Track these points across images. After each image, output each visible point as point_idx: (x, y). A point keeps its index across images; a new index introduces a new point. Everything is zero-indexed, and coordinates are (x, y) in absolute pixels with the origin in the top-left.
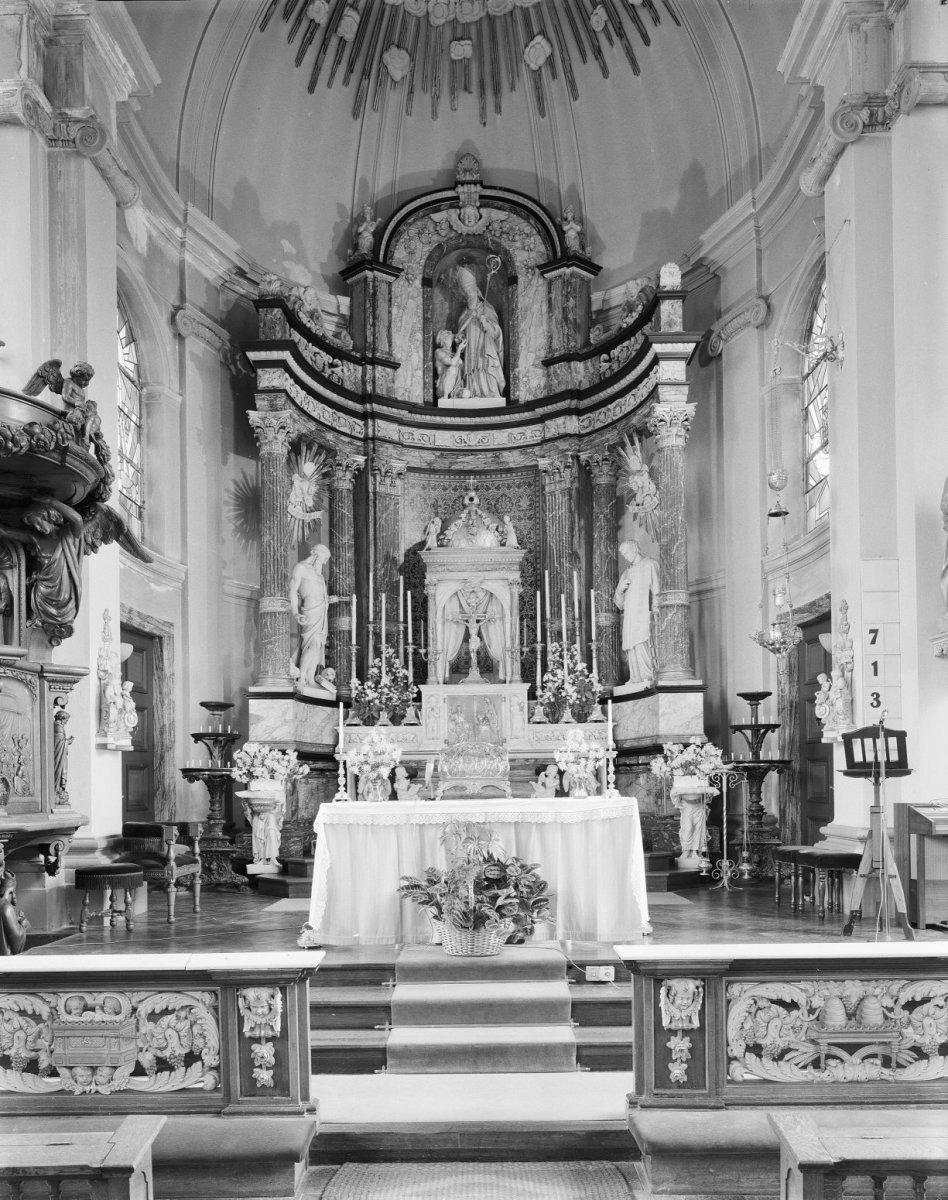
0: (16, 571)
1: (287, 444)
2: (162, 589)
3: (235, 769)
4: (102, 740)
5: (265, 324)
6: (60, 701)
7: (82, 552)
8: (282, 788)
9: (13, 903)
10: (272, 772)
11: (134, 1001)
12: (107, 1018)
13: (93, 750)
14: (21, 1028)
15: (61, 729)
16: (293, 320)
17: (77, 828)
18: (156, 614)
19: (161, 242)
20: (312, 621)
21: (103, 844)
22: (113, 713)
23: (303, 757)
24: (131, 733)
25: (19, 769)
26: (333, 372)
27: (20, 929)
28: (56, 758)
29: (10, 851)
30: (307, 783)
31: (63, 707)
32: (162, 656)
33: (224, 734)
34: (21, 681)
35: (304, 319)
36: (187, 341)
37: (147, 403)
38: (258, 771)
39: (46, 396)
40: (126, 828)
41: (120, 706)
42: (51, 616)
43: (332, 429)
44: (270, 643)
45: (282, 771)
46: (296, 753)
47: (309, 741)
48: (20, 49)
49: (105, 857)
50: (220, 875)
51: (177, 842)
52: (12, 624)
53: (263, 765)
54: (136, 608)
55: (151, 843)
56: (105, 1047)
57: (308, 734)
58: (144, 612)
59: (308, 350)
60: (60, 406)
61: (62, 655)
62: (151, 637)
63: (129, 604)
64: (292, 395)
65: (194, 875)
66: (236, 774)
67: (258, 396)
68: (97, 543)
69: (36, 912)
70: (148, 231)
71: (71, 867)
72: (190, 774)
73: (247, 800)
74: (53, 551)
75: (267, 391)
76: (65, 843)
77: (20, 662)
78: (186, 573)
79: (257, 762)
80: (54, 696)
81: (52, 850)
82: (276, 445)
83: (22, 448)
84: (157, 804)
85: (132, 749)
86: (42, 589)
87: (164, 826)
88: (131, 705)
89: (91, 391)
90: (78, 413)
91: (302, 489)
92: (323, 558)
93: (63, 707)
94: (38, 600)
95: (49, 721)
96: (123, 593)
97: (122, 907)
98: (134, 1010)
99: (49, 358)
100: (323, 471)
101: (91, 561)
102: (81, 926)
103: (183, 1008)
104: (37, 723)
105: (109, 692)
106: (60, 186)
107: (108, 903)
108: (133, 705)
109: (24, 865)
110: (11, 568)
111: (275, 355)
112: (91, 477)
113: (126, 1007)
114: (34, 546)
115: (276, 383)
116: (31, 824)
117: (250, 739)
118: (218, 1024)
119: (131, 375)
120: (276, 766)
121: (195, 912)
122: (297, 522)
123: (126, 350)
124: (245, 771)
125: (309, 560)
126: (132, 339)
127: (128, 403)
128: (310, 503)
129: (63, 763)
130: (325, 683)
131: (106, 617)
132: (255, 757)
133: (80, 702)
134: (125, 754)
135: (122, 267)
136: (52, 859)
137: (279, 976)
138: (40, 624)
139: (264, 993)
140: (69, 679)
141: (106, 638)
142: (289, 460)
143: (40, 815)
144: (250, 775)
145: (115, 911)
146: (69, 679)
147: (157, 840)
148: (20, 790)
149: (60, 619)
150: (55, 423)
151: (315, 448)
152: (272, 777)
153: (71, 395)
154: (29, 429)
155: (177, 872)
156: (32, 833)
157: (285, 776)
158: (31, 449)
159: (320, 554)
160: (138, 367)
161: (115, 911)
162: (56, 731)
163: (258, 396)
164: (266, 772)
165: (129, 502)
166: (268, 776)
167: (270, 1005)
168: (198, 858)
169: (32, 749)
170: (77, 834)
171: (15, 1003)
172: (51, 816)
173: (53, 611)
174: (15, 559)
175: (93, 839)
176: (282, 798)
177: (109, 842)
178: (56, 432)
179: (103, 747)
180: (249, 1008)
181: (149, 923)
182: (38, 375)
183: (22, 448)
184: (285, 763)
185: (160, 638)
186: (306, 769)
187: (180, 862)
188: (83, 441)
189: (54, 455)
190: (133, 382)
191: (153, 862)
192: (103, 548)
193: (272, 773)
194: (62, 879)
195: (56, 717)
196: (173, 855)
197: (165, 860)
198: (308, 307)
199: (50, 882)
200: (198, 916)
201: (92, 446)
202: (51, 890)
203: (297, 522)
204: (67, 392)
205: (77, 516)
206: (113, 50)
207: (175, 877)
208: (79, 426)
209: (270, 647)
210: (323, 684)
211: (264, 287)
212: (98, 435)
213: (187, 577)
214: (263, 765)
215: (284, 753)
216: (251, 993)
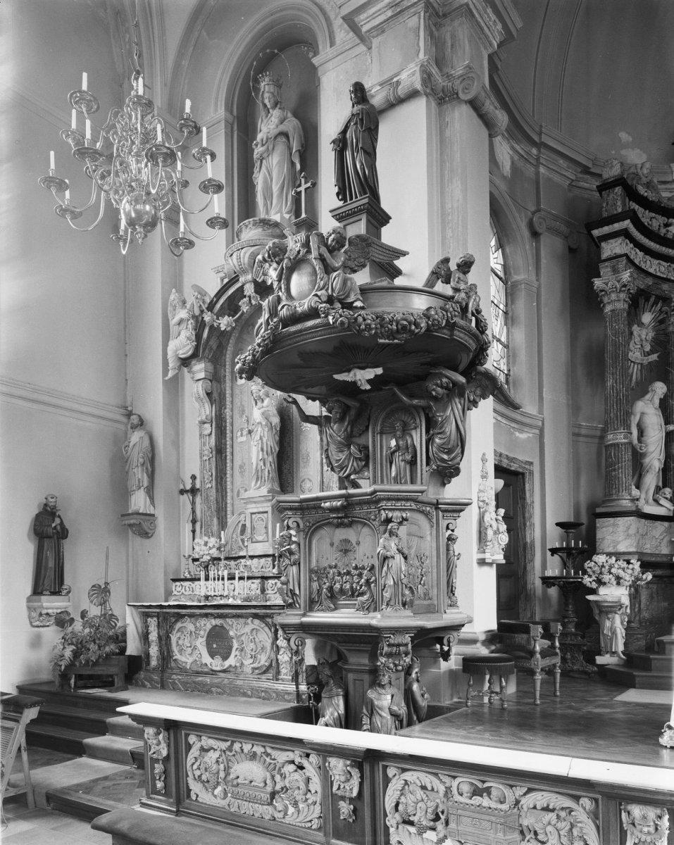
0: (419, 430)
1: (627, 299)
2: (523, 436)
3: (586, 576)
4: (481, 556)
5: (607, 204)
6: (450, 526)
7: (466, 409)
8: (627, 592)
9: (418, 681)
10: (618, 579)
11: (517, 795)
12: (494, 805)
13: (475, 564)
14: (423, 800)
15: (451, 548)
16: (632, 194)
17: (463, 625)
18: (523, 455)
19: (520, 164)
20: (651, 448)
21: (482, 637)
22: (490, 533)
23: (645, 566)
24: (503, 549)
25: (422, 579)
26: (668, 231)
27: (423, 702)
28: (448, 571)
29: (416, 642)
30: (647, 588)
31: (453, 531)
32: (524, 488)
33: (576, 548)
34: (422, 512)
35: (642, 190)
36: (542, 239)
37: (511, 292)
38: (606, 578)
39: (440, 287)
40: (499, 624)
41: (495, 528)
42: (443, 460)
43: (667, 280)
44: (615, 470)
45: (628, 578)
46: (639, 563)
47: (649, 551)
48: (419, 39)
49: (484, 648)
50: (573, 663)
51: (542, 638)
52: (417, 468)
53: (610, 573)
54: (505, 452)
55: (520, 638)
56: (492, 831)
57: (648, 546)
58: (511, 455)
59: (645, 216)
60: (449, 292)
61: (452, 491)
62: (516, 474)
63: (499, 450)
64: (632, 257)
65: (554, 665)
66: (587, 580)
67: (601, 265)
68: (477, 400)
69: (433, 689)
70: (512, 158)
71: (461, 655)
72: (547, 581)
73: (596, 602)
74: (445, 411)
75: (609, 259)
76: (454, 636)
77: (422, 497)
78: (543, 422)
79: (605, 570)
80: (446, 522)
81: (445, 641)
82: (616, 303)
83: (422, 328)
84: (522, 605)
85: (504, 562)
86: (437, 440)
87: (531, 625)
88: (503, 527)
89: (472, 277)
90: (463, 295)
91: (640, 336)
92: (660, 393)
93: (453, 531)
94: (434, 449)
95: (443, 541)
96: (496, 442)
97: (498, 690)
98: (517, 802)
99: (441, 258)
100: (660, 318)
101: (473, 414)
102: (467, 702)
103: (563, 809)
104: (434, 545)
105: (487, 518)
106: (448, 133)
107: (487, 685)
108: (505, 527)
109: (425, 652)
110: (415, 428)
111: (617, 226)
112: (472, 345)
113: (510, 798)
114: (430, 408)
115: (618, 251)
116: (429, 622)
117: (597, 552)
118: (599, 834)
119: (499, 273)
120: (621, 573)
121: (556, 696)
122: (636, 366)
123: (496, 255)
124: (594, 578)
125: (648, 396)
126: (500, 245)
127: (497, 296)
128: (648, 348)
129: (453, 574)
130: (663, 502)
131: (484, 460)
132: (603, 566)
133: (466, 526)
134: (499, 566)
135: (496, 193)
136: (446, 648)
137: (669, 798)
138: (436, 468)
139: (651, 812)
140: (457, 508)
141: (484, 477)
142: (629, 313)
143: (436, 615)
144: (600, 582)
145: (492, 692)
146: (457, 508)
147: (525, 636)
148: (422, 596)
149: (450, 463)
150: (446, 305)
151: (652, 299)
152: (618, 584)
153: (458, 282)
154: (426, 315)
155: (539, 662)
156: (431, 629)
157: (631, 582)
158: (428, 329)
159: (658, 390)
160: (505, 267)
161: (492, 692)
162: (448, 550)
163: (601, 265)
164: (613, 579)
165: (498, 372)
166: (615, 583)
167: (656, 825)
168: (558, 651)
169: (430, 562)
170: (463, 629)
171: (418, 778)
172: (444, 616)
173: (445, 457)
174: (418, 421)
175: (475, 633)
176: (626, 601)
177: (487, 635)
178: (447, 312)
179: (482, 562)
180: (633, 824)
181: (518, 703)
182: (433, 273)
183: (422, 328)
184: (630, 571)
185: (523, 474)
186: (649, 576)
187: (544, 654)
188: (466, 317)
189: (445, 331)
190: (500, 279)
191: (522, 654)
192: (482, 403)
193: (618, 580)
194: (453, 663)
195: (447, 538)
196: (538, 648)
197: (532, 653)
198: (644, 180)
199: (444, 666)
200: (558, 700)
201: (474, 319)
202: (445, 672)
203: (636, 366)
204: (454, 280)
205: (462, 379)
206: (486, 12)
207: (540, 667)
208: (464, 304)
209: (614, 473)
210: (661, 502)
211: (605, 176)
212: (478, 311)
213: (543, 424)
214: (610, 573)
215: (628, 562)
216: (637, 811)
